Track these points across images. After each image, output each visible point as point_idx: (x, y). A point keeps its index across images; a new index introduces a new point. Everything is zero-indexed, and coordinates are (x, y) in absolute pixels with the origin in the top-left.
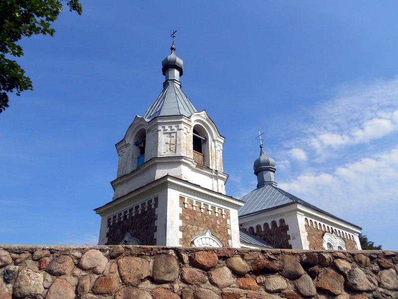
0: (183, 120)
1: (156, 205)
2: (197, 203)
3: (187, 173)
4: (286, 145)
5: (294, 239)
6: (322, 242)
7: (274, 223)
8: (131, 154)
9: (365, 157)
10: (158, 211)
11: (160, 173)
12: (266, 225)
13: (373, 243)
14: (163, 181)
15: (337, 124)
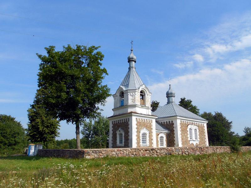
0: (137, 91)
1: (129, 121)
2: (141, 119)
3: (138, 110)
4: (191, 52)
5: (175, 128)
6: (187, 128)
7: (169, 122)
8: (119, 99)
9: (243, 59)
10: (129, 123)
11: (130, 110)
12: (164, 122)
13: (228, 120)
14: (131, 114)
15: (223, 39)
